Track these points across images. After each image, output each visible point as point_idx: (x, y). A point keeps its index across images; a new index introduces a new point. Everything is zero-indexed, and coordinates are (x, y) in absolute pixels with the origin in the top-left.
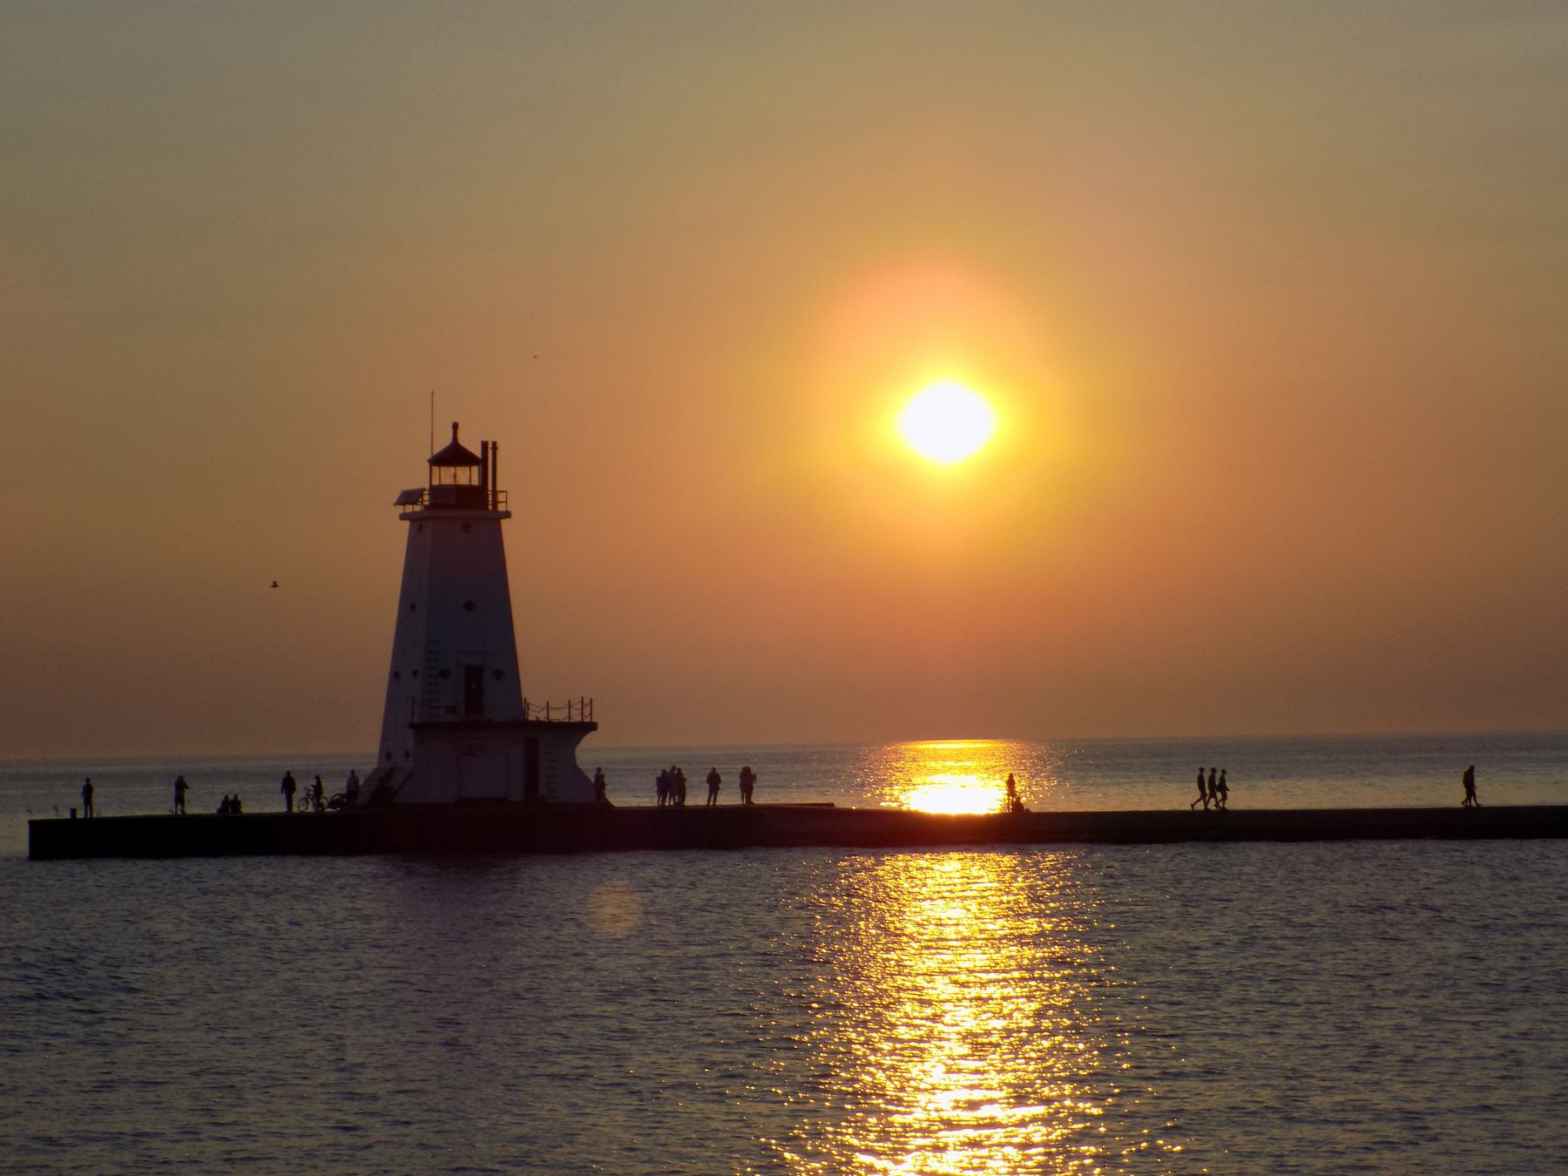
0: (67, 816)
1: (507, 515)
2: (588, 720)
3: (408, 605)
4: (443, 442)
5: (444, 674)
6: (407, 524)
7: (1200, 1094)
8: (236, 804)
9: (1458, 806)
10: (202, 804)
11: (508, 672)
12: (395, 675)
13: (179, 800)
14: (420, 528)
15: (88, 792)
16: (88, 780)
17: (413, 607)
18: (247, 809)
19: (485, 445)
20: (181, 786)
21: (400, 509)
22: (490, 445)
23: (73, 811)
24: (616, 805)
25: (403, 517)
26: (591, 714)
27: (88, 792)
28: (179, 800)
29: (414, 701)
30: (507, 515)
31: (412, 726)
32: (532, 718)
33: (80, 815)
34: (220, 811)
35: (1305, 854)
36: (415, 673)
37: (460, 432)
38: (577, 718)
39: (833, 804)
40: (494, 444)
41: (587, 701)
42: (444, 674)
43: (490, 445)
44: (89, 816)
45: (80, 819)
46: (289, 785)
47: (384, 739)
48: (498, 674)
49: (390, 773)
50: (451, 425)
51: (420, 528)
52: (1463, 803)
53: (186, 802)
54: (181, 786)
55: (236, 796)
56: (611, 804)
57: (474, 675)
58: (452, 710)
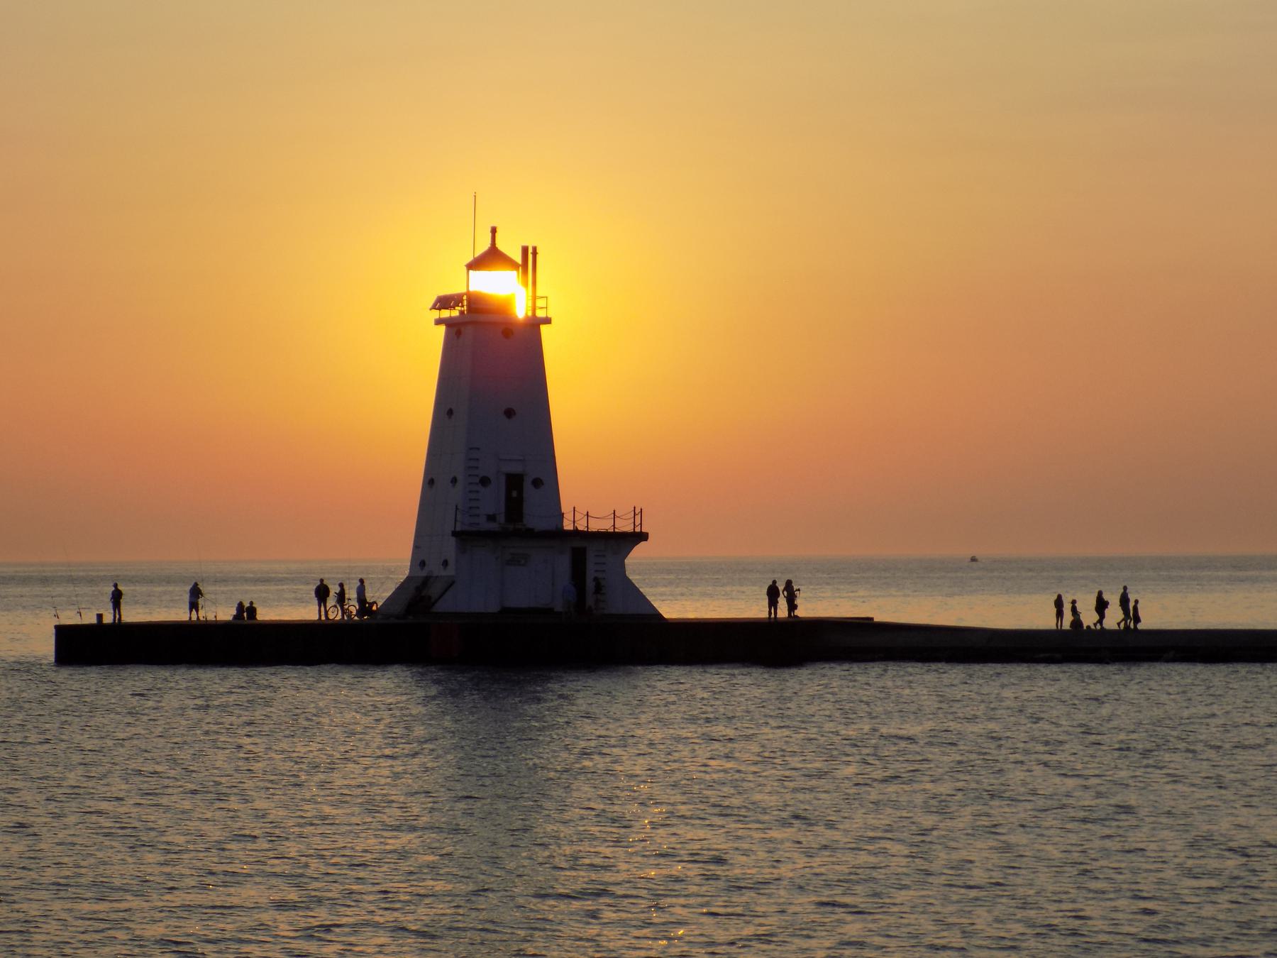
0: (94, 621)
1: (547, 321)
2: (638, 530)
3: (445, 410)
4: (483, 246)
5: (485, 481)
6: (442, 328)
7: (35, 727)
8: (252, 611)
9: (1112, 628)
10: (220, 611)
11: (546, 479)
12: (429, 482)
13: (194, 606)
14: (459, 333)
15: (117, 597)
16: (116, 586)
17: (450, 412)
18: (264, 615)
19: (525, 250)
20: (196, 593)
21: (436, 314)
22: (530, 251)
23: (100, 616)
24: (666, 616)
25: (439, 322)
26: (641, 524)
27: (117, 597)
28: (194, 606)
29: (457, 509)
30: (547, 321)
31: (455, 534)
32: (568, 526)
33: (108, 619)
34: (235, 617)
35: (1217, 674)
36: (454, 481)
37: (498, 235)
38: (628, 528)
39: (872, 619)
40: (535, 249)
41: (638, 511)
42: (485, 481)
43: (530, 251)
44: (773, 616)
45: (108, 626)
46: (322, 593)
47: (416, 547)
48: (537, 483)
49: (426, 581)
50: (490, 230)
51: (459, 333)
52: (1119, 624)
53: (200, 606)
54: (196, 593)
55: (251, 603)
56: (661, 616)
57: (514, 482)
58: (491, 518)
